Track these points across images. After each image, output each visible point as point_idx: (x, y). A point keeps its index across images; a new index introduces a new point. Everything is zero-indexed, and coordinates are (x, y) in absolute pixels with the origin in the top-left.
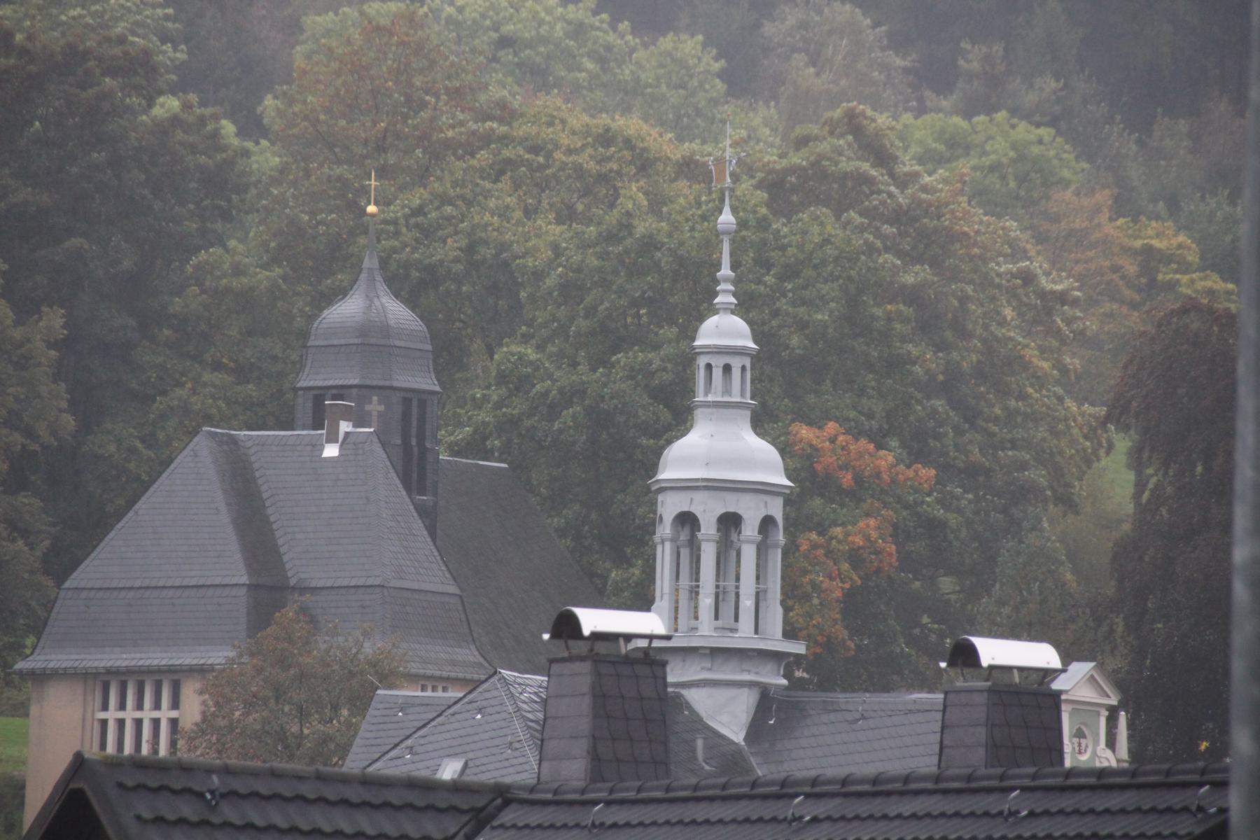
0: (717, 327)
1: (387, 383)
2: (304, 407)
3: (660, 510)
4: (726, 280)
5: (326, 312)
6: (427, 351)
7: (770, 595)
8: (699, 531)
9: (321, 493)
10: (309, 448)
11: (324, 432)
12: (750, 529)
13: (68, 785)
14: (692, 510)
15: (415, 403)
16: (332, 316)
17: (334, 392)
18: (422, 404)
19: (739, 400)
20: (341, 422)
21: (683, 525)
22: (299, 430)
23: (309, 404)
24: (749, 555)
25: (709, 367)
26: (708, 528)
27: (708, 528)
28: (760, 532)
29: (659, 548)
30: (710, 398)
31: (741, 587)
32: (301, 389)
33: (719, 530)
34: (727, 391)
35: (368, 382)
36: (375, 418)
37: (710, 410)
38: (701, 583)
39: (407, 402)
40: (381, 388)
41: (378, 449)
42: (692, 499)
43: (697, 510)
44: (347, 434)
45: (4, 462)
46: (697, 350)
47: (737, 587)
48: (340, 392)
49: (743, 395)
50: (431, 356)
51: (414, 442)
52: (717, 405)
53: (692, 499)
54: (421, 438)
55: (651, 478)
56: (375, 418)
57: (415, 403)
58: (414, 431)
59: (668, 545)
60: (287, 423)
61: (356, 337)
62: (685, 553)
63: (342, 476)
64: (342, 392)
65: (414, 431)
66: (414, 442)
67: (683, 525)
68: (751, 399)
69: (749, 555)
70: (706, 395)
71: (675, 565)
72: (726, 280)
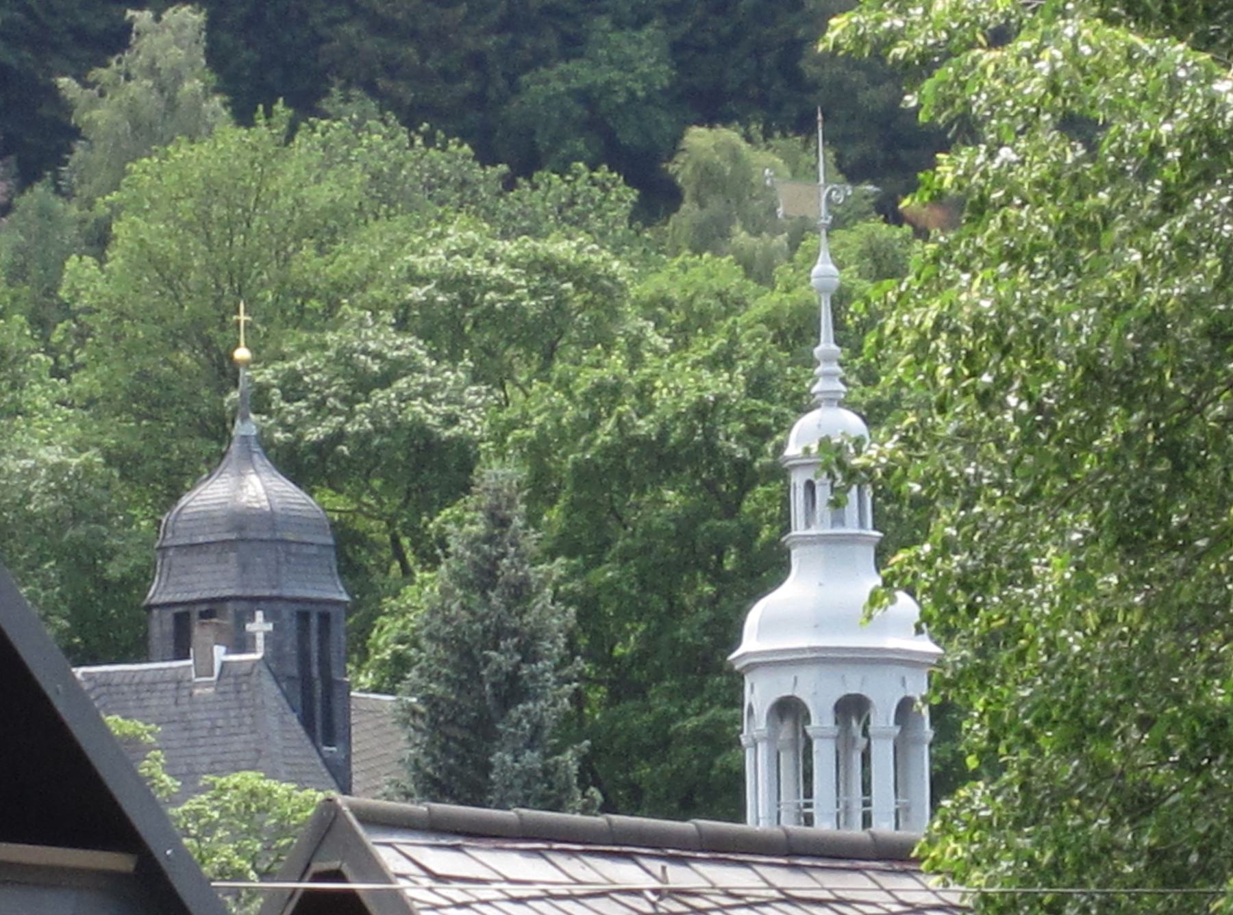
0: (819, 426)
1: (275, 592)
2: (161, 628)
3: (748, 697)
4: (828, 359)
5: (184, 501)
6: (325, 546)
7: (914, 811)
8: (809, 723)
9: (192, 746)
10: (172, 686)
11: (190, 662)
12: (883, 718)
13: (308, 866)
14: (797, 694)
15: (314, 621)
16: (192, 504)
17: (204, 608)
18: (325, 618)
19: (857, 531)
20: (216, 648)
21: (782, 719)
22: (158, 661)
23: (169, 627)
24: (883, 755)
25: (810, 486)
26: (821, 721)
27: (821, 721)
28: (896, 723)
29: (749, 754)
30: (813, 531)
31: (874, 802)
32: (157, 606)
33: (836, 722)
34: (838, 520)
35: (249, 592)
36: (260, 642)
37: (811, 549)
38: (815, 801)
39: (304, 617)
40: (270, 599)
41: (268, 684)
42: (796, 679)
43: (804, 694)
44: (224, 665)
45: (956, 8)
46: (791, 463)
47: (867, 804)
48: (211, 608)
49: (862, 524)
50: (333, 554)
51: (315, 670)
52: (825, 540)
53: (796, 679)
54: (325, 663)
55: (732, 651)
56: (260, 642)
57: (314, 621)
58: (315, 656)
59: (762, 748)
60: (138, 650)
61: (228, 532)
62: (786, 759)
63: (220, 722)
64: (215, 606)
65: (315, 656)
66: (315, 670)
67: (782, 719)
68: (875, 528)
69: (883, 755)
70: (808, 526)
71: (775, 778)
72: (828, 359)
